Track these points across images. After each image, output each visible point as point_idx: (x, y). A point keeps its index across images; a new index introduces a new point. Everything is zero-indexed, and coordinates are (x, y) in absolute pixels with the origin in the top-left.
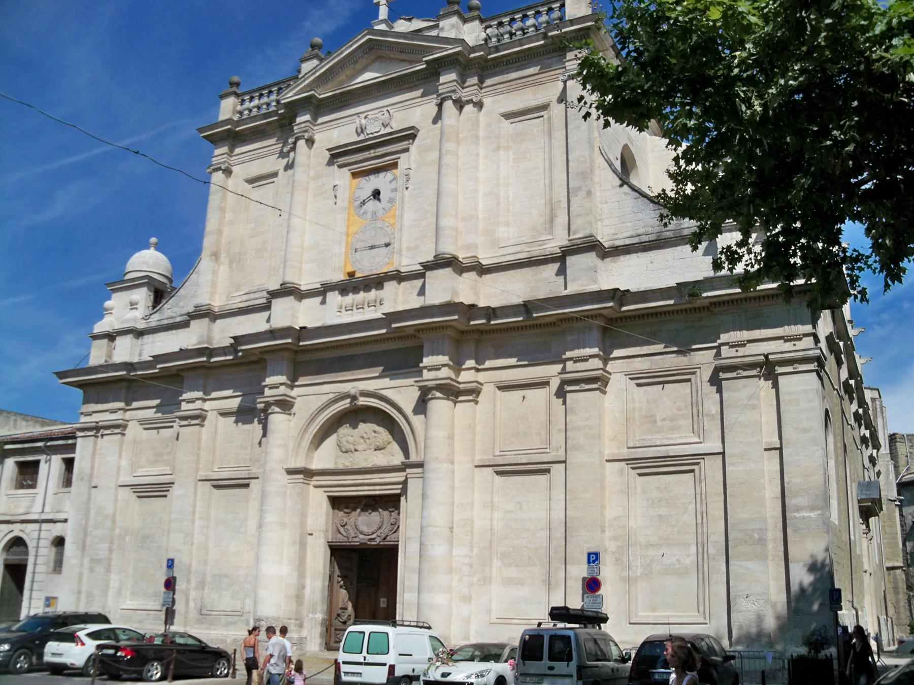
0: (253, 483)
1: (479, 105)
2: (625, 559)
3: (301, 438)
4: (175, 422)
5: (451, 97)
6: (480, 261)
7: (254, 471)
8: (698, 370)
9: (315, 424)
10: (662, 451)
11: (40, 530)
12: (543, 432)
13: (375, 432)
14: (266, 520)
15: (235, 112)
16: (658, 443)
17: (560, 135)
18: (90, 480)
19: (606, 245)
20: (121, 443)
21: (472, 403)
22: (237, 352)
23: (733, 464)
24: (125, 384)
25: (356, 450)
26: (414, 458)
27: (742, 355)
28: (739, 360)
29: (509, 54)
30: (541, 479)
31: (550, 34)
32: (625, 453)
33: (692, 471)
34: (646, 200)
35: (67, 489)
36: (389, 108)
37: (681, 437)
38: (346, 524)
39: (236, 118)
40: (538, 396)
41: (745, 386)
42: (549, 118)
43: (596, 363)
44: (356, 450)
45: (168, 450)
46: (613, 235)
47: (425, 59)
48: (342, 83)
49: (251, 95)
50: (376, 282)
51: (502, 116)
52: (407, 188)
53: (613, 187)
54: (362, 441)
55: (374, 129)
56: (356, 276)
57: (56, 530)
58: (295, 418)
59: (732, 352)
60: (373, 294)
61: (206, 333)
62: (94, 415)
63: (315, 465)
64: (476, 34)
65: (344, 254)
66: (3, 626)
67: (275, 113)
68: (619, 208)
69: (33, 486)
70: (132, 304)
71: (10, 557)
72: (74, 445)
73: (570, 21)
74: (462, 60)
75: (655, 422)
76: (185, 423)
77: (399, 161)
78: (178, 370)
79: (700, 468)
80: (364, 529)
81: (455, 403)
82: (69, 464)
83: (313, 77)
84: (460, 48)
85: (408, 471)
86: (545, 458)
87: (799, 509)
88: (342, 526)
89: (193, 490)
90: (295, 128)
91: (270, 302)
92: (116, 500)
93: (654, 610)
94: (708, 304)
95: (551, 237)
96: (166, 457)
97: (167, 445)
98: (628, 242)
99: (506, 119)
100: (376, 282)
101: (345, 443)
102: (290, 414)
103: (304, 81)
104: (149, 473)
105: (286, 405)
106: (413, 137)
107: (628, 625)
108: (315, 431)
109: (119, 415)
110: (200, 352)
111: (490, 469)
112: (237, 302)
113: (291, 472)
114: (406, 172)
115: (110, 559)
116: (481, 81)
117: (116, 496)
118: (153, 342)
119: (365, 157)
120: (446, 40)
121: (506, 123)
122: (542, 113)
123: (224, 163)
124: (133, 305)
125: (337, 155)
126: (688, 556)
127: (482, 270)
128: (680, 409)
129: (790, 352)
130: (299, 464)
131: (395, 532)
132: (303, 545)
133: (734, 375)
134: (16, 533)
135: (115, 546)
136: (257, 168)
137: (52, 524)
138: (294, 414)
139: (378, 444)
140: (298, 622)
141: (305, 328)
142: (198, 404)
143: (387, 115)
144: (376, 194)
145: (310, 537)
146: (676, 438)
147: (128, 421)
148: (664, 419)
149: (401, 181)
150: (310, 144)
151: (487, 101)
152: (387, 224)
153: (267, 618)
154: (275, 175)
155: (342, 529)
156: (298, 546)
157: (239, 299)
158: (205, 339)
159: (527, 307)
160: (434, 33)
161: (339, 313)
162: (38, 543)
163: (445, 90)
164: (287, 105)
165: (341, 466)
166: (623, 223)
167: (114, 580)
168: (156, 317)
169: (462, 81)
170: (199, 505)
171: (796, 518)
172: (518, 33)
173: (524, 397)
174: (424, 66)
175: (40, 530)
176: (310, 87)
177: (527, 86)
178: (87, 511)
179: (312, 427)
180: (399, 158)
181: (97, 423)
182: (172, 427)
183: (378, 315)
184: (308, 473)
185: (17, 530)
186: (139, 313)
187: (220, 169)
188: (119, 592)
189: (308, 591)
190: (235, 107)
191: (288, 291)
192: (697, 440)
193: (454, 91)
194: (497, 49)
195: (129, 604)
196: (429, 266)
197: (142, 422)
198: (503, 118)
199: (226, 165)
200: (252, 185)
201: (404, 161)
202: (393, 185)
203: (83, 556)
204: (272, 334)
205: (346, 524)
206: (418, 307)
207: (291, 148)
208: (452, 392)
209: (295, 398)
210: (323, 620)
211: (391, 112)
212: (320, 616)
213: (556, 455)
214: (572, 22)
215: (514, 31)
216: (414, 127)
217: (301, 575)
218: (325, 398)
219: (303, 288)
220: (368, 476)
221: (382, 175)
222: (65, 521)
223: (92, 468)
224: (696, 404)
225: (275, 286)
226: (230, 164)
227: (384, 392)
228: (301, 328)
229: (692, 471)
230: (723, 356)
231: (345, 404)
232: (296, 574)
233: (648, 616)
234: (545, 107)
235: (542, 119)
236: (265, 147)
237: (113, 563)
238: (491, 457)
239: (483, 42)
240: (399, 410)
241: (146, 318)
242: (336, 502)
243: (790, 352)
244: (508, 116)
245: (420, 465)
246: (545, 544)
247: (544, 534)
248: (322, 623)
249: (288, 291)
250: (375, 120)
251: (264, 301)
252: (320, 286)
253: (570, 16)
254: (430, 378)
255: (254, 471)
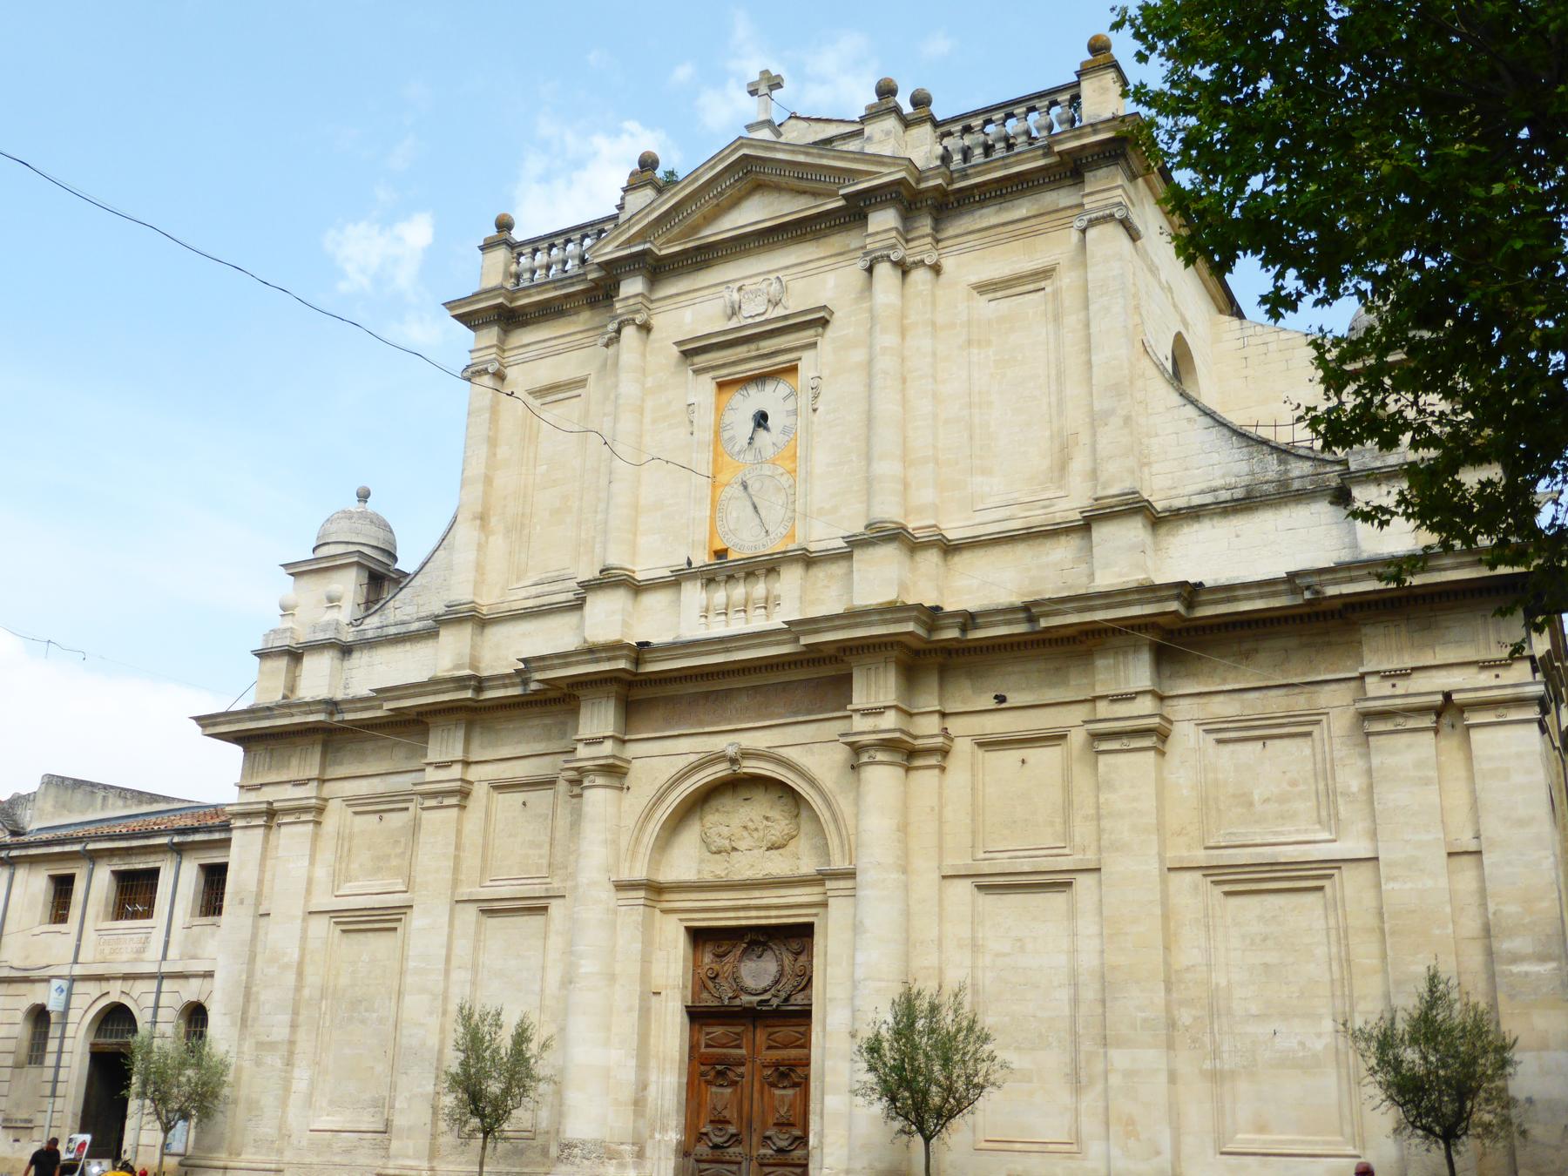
0: (554, 905)
1: (936, 269)
2: (1207, 1039)
3: (640, 830)
4: (411, 800)
5: (888, 257)
6: (944, 533)
7: (556, 884)
8: (1324, 718)
9: (664, 806)
10: (1267, 854)
11: (159, 992)
12: (1058, 820)
13: (767, 818)
14: (582, 970)
15: (508, 274)
16: (1259, 841)
17: (1072, 320)
18: (258, 904)
19: (1159, 506)
20: (315, 838)
21: (936, 772)
22: (525, 683)
23: (1394, 879)
24: (320, 737)
25: (734, 849)
26: (838, 864)
27: (1403, 692)
28: (1398, 701)
29: (984, 184)
30: (1057, 900)
31: (1057, 149)
32: (1201, 857)
33: (1321, 888)
34: (1225, 431)
35: (211, 919)
36: (780, 274)
37: (1298, 831)
38: (717, 975)
39: (510, 284)
40: (1042, 757)
41: (1409, 746)
42: (1056, 293)
43: (1146, 705)
44: (734, 849)
45: (399, 850)
46: (1170, 489)
47: (842, 192)
48: (695, 229)
49: (535, 245)
50: (768, 567)
51: (974, 288)
52: (815, 410)
53: (1168, 409)
54: (745, 834)
55: (755, 309)
56: (730, 558)
57: (191, 991)
58: (629, 796)
59: (1385, 688)
60: (759, 589)
61: (467, 651)
62: (265, 789)
63: (667, 875)
64: (926, 148)
65: (708, 520)
66: (58, 1172)
67: (580, 278)
68: (1178, 445)
69: (148, 914)
70: (330, 600)
71: (102, 1040)
72: (229, 840)
73: (1092, 125)
74: (904, 193)
75: (1251, 804)
76: (433, 803)
77: (800, 364)
78: (419, 714)
79: (1334, 886)
80: (749, 983)
81: (908, 770)
82: (215, 877)
83: (645, 222)
84: (902, 175)
85: (829, 884)
86: (1065, 864)
87: (1516, 958)
88: (711, 978)
89: (446, 918)
90: (618, 305)
91: (584, 600)
92: (304, 938)
93: (1261, 1129)
94: (1340, 606)
95: (1062, 494)
96: (394, 862)
97: (397, 842)
98: (1196, 501)
99: (981, 293)
100: (768, 567)
101: (716, 838)
102: (621, 789)
103: (629, 228)
104: (364, 890)
105: (614, 772)
106: (824, 323)
107: (1218, 1156)
108: (664, 817)
109: (309, 791)
110: (461, 683)
111: (968, 882)
112: (519, 599)
113: (621, 886)
114: (813, 383)
115: (292, 1043)
116: (936, 229)
117: (304, 931)
118: (370, 665)
119: (742, 356)
120: (878, 159)
121: (981, 301)
122: (1042, 284)
123: (491, 361)
124: (333, 601)
125: (691, 352)
126: (1319, 1035)
127: (949, 548)
128: (1293, 783)
129: (1490, 688)
130: (640, 873)
131: (803, 989)
132: (645, 1013)
133: (1389, 726)
134: (115, 997)
135: (301, 1018)
136: (545, 372)
137: (181, 982)
138: (628, 788)
139: (774, 838)
140: (636, 1148)
141: (647, 644)
142: (456, 771)
143: (776, 286)
144: (761, 419)
145: (654, 999)
146: (1290, 833)
147: (326, 800)
148: (1267, 800)
149: (804, 400)
150: (644, 332)
151: (948, 263)
152: (780, 470)
153: (584, 1143)
154: (580, 383)
155: (710, 984)
156: (636, 1015)
157: (523, 593)
158: (467, 660)
159: (1029, 611)
160: (853, 146)
161: (703, 620)
162: (155, 1015)
163: (878, 245)
164: (607, 266)
165: (708, 877)
166: (1186, 469)
167: (301, 1079)
168: (373, 621)
169: (906, 234)
170: (462, 947)
171: (1512, 974)
172: (998, 146)
173: (1023, 761)
174: (841, 203)
175: (159, 992)
176: (642, 235)
177: (1016, 238)
178: (252, 959)
179: (659, 812)
180: (800, 359)
181: (270, 803)
182: (407, 809)
183: (776, 622)
184: (655, 889)
185: (115, 993)
186: (345, 613)
187: (485, 371)
188: (309, 1102)
189: (652, 1091)
190: (507, 266)
191: (610, 580)
192: (1326, 836)
193: (893, 247)
194: (966, 177)
195: (326, 1122)
196: (856, 543)
197: (350, 801)
198: (975, 292)
199: (496, 365)
200: (540, 401)
201: (808, 364)
202: (790, 404)
203: (242, 1038)
204: (592, 651)
205: (717, 975)
206: (842, 611)
207: (610, 339)
208: (906, 753)
209: (629, 762)
210: (679, 1143)
211: (784, 280)
212: (673, 1136)
213: (1081, 860)
214: (1094, 127)
215: (990, 142)
216: (825, 306)
217: (642, 1066)
218: (681, 763)
219: (639, 577)
220: (757, 894)
221: (770, 387)
222: (209, 975)
223: (260, 882)
224: (1325, 773)
225: (589, 572)
226: (501, 364)
227: (785, 752)
228: (641, 644)
229: (1321, 888)
230: (1370, 694)
231: (720, 771)
232: (633, 1063)
233: (1253, 1141)
234: (1046, 273)
235: (1042, 293)
236: (555, 338)
237: (298, 1049)
238: (970, 862)
239: (938, 163)
240: (812, 782)
241: (356, 622)
242: (699, 937)
243: (1490, 688)
244: (983, 288)
245: (850, 875)
246: (1067, 1011)
247: (1064, 995)
248: (676, 1151)
249: (610, 580)
250: (757, 293)
251: (571, 596)
252: (670, 574)
253: (1089, 117)
254: (866, 729)
255: (555, 885)
